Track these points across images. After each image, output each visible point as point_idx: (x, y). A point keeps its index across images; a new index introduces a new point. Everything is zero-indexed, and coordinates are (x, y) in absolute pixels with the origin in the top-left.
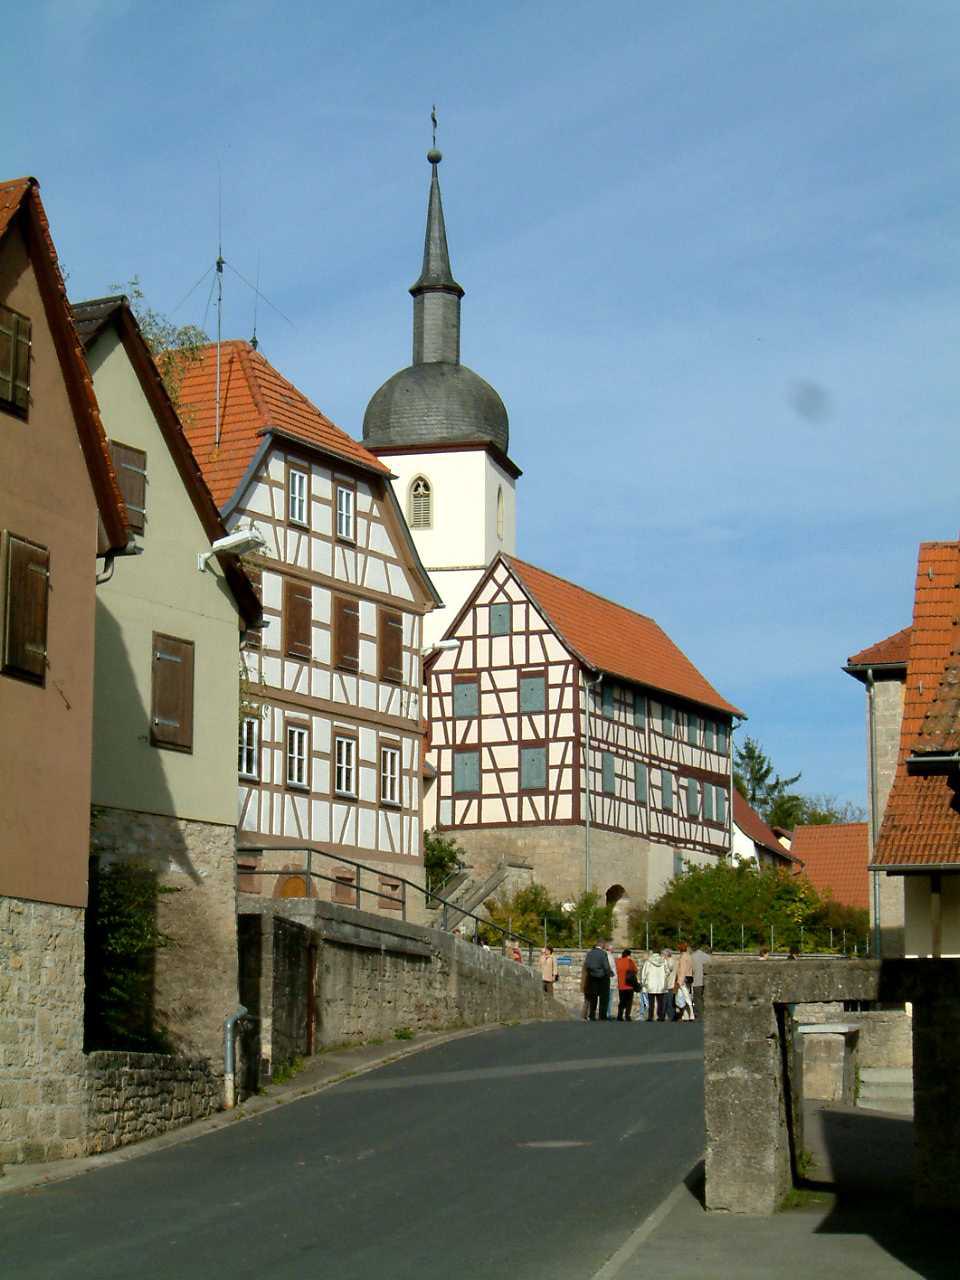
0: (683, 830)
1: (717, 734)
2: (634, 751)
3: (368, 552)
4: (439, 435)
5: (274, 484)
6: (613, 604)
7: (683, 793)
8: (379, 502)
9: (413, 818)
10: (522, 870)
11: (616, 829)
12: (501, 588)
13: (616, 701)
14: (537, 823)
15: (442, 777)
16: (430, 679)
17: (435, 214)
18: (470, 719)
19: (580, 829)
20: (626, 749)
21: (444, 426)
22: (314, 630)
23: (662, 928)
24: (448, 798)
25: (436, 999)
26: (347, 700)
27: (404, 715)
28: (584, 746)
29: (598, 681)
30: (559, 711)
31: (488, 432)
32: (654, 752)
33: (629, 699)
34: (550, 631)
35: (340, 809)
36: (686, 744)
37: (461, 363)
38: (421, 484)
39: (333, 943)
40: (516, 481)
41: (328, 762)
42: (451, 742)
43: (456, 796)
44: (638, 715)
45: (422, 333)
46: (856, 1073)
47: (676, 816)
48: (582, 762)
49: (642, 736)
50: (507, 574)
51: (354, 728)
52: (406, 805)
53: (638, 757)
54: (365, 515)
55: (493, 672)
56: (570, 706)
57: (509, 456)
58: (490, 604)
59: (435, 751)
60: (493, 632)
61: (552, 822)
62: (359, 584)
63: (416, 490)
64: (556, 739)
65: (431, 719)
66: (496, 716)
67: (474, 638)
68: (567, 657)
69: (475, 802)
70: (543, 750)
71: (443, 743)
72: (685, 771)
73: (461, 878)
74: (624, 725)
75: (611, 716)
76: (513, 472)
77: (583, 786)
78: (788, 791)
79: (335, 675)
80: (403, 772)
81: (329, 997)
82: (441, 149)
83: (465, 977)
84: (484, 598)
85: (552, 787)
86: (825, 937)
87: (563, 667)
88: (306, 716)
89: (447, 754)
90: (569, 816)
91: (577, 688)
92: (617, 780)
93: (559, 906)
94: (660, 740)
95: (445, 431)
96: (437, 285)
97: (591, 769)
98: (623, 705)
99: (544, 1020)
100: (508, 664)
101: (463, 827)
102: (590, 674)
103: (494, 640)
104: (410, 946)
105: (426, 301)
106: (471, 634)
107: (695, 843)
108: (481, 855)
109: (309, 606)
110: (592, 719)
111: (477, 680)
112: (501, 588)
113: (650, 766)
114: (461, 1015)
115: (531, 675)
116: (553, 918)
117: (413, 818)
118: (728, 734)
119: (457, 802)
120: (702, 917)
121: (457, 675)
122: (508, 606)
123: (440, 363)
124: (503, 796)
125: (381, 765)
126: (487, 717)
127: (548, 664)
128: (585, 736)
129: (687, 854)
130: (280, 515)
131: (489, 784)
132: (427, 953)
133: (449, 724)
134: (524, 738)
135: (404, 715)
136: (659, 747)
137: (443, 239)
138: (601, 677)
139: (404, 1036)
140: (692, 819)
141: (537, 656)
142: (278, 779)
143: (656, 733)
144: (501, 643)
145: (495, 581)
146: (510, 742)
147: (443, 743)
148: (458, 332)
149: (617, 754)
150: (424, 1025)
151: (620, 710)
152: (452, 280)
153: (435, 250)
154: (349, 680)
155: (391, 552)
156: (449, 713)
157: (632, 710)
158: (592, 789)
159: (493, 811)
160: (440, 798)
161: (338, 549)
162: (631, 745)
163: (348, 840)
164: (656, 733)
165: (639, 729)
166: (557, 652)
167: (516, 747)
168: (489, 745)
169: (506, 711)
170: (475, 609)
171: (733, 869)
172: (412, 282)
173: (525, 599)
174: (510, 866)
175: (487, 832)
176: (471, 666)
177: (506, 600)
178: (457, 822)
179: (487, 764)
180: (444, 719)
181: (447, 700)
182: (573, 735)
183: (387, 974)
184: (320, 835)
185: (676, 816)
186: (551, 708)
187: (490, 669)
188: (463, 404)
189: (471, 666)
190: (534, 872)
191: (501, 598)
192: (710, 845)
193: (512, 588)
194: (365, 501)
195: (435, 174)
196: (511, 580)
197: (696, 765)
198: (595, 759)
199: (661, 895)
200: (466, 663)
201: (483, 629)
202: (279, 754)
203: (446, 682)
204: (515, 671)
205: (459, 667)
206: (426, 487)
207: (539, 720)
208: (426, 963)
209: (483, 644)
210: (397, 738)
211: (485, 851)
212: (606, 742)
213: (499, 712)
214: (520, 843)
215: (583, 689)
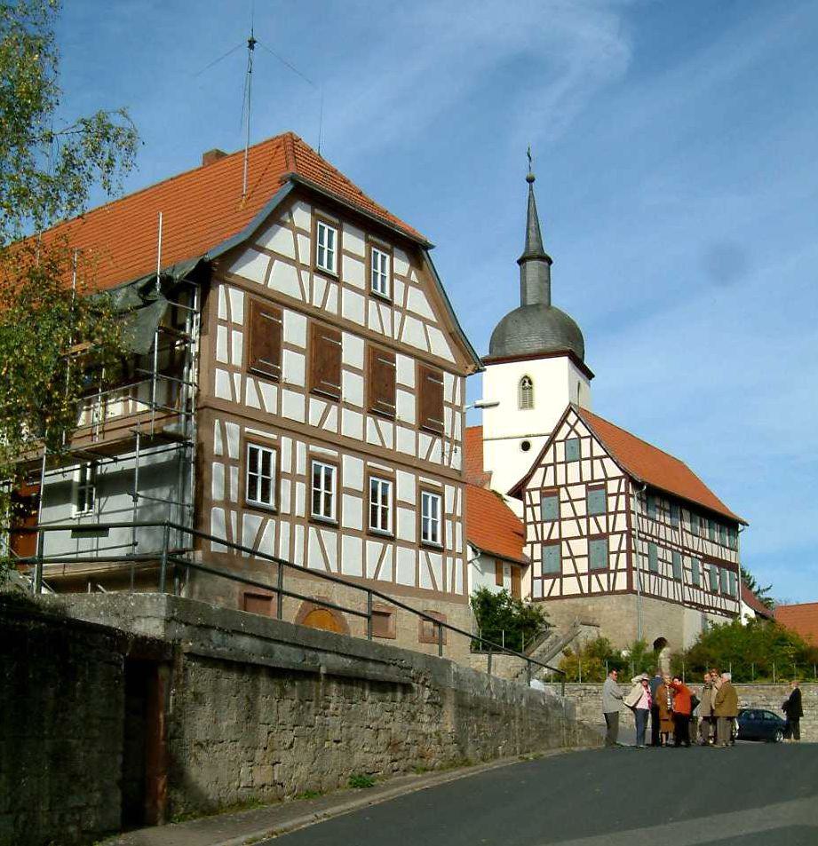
0: (708, 600)
1: (729, 535)
3: (405, 311)
5: (297, 231)
7: (706, 574)
9: (457, 560)
10: (592, 627)
11: (659, 598)
12: (572, 428)
14: (602, 593)
15: (535, 564)
16: (525, 495)
17: (532, 214)
18: (553, 522)
19: (632, 596)
20: (665, 541)
22: (344, 372)
23: (694, 667)
24: (539, 578)
25: (423, 734)
26: (383, 442)
27: (446, 464)
30: (616, 512)
31: (571, 347)
32: (685, 545)
34: (608, 456)
35: (374, 546)
36: (708, 540)
37: (552, 304)
39: (208, 660)
42: (540, 539)
43: (545, 576)
47: (702, 590)
48: (633, 548)
52: (449, 546)
54: (402, 278)
55: (569, 488)
56: (624, 509)
57: (585, 363)
58: (565, 440)
59: (529, 546)
61: (613, 592)
62: (396, 338)
64: (614, 533)
65: (526, 523)
67: (555, 464)
68: (621, 474)
69: (558, 580)
70: (605, 541)
72: (707, 559)
73: (547, 634)
77: (634, 565)
78: (763, 596)
79: (368, 418)
80: (446, 517)
81: (201, 737)
82: (535, 174)
83: (467, 708)
84: (561, 436)
85: (612, 567)
86: (811, 671)
88: (334, 453)
89: (538, 547)
90: (625, 588)
91: (628, 496)
92: (660, 563)
93: (619, 653)
94: (690, 536)
96: (534, 256)
97: (640, 553)
99: (577, 749)
100: (579, 481)
101: (550, 598)
103: (569, 465)
104: (373, 670)
106: (552, 462)
107: (716, 609)
108: (562, 617)
109: (340, 349)
110: (640, 518)
111: (557, 494)
112: (572, 428)
114: (462, 751)
115: (595, 488)
116: (614, 661)
117: (457, 560)
118: (736, 537)
119: (545, 581)
120: (724, 659)
121: (544, 491)
123: (537, 305)
124: (577, 575)
125: (420, 508)
126: (565, 519)
127: (607, 479)
128: (634, 530)
129: (710, 616)
130: (305, 258)
131: (568, 567)
132: (406, 680)
133: (539, 526)
134: (591, 533)
135: (446, 464)
136: (690, 541)
137: (538, 228)
139: (363, 782)
140: (714, 592)
141: (599, 474)
142: (300, 510)
143: (687, 532)
144: (573, 467)
145: (568, 424)
146: (582, 537)
149: (659, 544)
150: (402, 767)
153: (532, 234)
155: (429, 314)
156: (538, 519)
157: (669, 514)
158: (641, 568)
159: (571, 586)
160: (533, 578)
161: (372, 304)
163: (385, 575)
164: (687, 532)
165: (675, 528)
166: (613, 471)
167: (586, 540)
168: (567, 539)
170: (554, 444)
171: (741, 625)
174: (581, 624)
175: (566, 601)
178: (546, 595)
179: (566, 553)
180: (535, 523)
181: (537, 509)
183: (332, 705)
184: (351, 568)
185: (702, 590)
187: (566, 485)
188: (553, 328)
190: (600, 629)
191: (573, 435)
193: (581, 428)
194: (402, 266)
195: (531, 189)
196: (579, 422)
197: (715, 555)
198: (643, 547)
199: (693, 644)
200: (549, 482)
201: (561, 458)
202: (301, 488)
203: (536, 496)
206: (530, 382)
207: (602, 519)
208: (404, 693)
209: (561, 468)
210: (439, 484)
211: (565, 615)
213: (573, 515)
214: (590, 608)
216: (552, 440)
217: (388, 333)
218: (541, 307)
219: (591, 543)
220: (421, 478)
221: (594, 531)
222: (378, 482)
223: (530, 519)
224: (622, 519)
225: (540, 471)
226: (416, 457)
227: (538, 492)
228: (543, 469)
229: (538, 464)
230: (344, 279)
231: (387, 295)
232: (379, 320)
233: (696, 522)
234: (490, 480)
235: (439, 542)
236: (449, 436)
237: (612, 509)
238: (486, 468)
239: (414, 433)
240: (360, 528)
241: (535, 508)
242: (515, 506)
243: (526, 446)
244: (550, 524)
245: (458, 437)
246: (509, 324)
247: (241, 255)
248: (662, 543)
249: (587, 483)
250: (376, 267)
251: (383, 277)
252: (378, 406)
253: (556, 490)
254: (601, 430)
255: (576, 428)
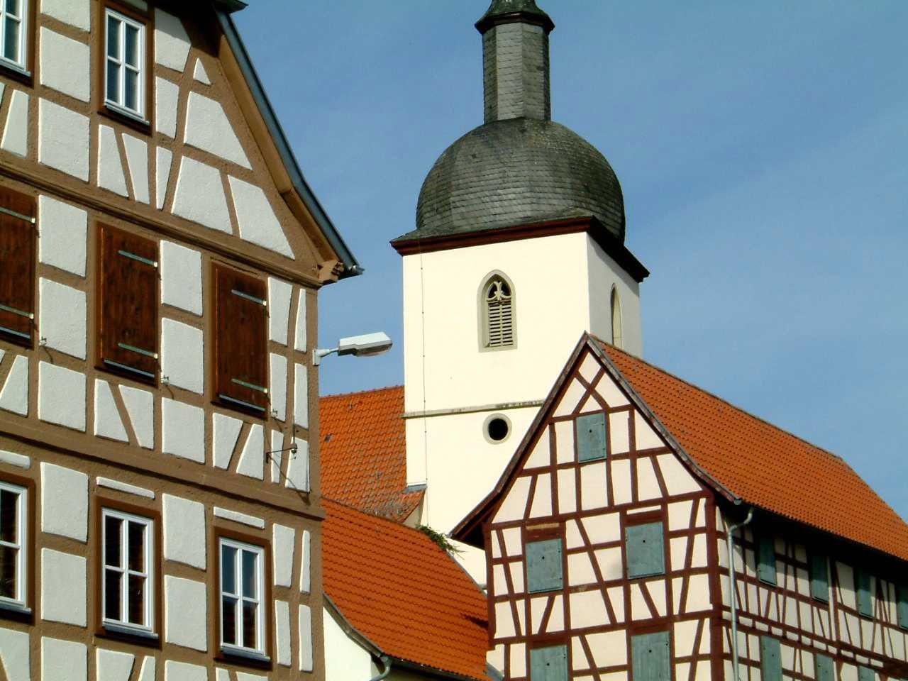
2: (812, 636)
3: (179, 147)
4: (521, 215)
6: (776, 428)
8: (207, 56)
12: (591, 389)
13: (778, 557)
16: (490, 538)
18: (551, 594)
20: (799, 631)
21: (528, 200)
22: (43, 284)
27: (274, 477)
28: (728, 624)
29: (746, 522)
30: (688, 572)
33: (801, 557)
34: (668, 449)
35: (113, 661)
36: (896, 628)
37: (555, 117)
38: (499, 285)
40: (640, 283)
41: (83, 560)
42: (524, 633)
44: (815, 582)
45: (495, 80)
46: (409, 528)
48: (726, 649)
49: (824, 613)
50: (598, 367)
51: (150, 494)
52: (282, 657)
53: (817, 644)
54: (171, 75)
56: (704, 564)
58: (575, 415)
59: (500, 648)
60: (581, 458)
63: (491, 294)
64: (684, 616)
66: (590, 587)
67: (553, 468)
68: (695, 487)
71: (513, 634)
74: (796, 595)
75: (771, 580)
76: (636, 272)
84: (566, 406)
87: (690, 503)
88: (22, 460)
89: (519, 650)
91: (713, 536)
94: (853, 620)
95: (527, 207)
97: (741, 660)
98: (792, 565)
102: (733, 512)
103: (583, 469)
105: (498, 36)
109: (33, 232)
110: (741, 584)
111: (560, 534)
112: (591, 389)
113: (840, 659)
122: (603, 415)
123: (520, 120)
125: (217, 573)
126: (576, 589)
127: (666, 500)
128: (728, 609)
133: (521, 604)
135: (274, 477)
136: (854, 631)
138: (750, 515)
141: (648, 490)
144: (594, 475)
145: (581, 380)
146: (613, 626)
147: (513, 634)
148: (547, 77)
151: (786, 573)
152: (536, 7)
154: (136, 397)
155: (236, 153)
156: (519, 588)
157: (805, 573)
161: (106, 131)
162: (806, 626)
165: (819, 603)
166: (680, 480)
168: (582, 633)
169: (585, 555)
172: (480, 14)
173: (628, 403)
176: (550, 514)
177: (599, 408)
179: (580, 662)
180: (512, 597)
181: (517, 569)
182: (710, 607)
186: (674, 568)
187: (579, 515)
188: (555, 169)
189: (550, 514)
191: (592, 405)
192: (612, 347)
193: (610, 392)
196: (605, 376)
200: (542, 508)
201: (566, 453)
204: (617, 515)
205: (532, 516)
206: (506, 289)
209: (565, 477)
210: (259, 522)
212: (765, 620)
215: (723, 535)
216: (546, 419)
217: (141, 195)
218: (527, 123)
219: (635, 639)
220: (217, 511)
221: (641, 612)
222: (120, 521)
223: (500, 588)
224: (700, 584)
225: (522, 483)
226: (205, 465)
227: (517, 532)
228: (528, 479)
229: (516, 469)
230: (42, 79)
231: (140, 111)
232: (120, 167)
233: (867, 588)
234: (420, 504)
235: (260, 648)
236: (281, 416)
237: (678, 563)
238: (413, 479)
239: (200, 412)
240: (82, 621)
241: (512, 565)
242: (471, 560)
243: (498, 430)
244: (545, 599)
245: (301, 417)
246: (460, 164)
247: (206, 52)
248: (791, 635)
249: (622, 509)
250: (113, 52)
251: (131, 75)
252: (119, 354)
253: (557, 525)
254: (650, 390)
255: (598, 389)
